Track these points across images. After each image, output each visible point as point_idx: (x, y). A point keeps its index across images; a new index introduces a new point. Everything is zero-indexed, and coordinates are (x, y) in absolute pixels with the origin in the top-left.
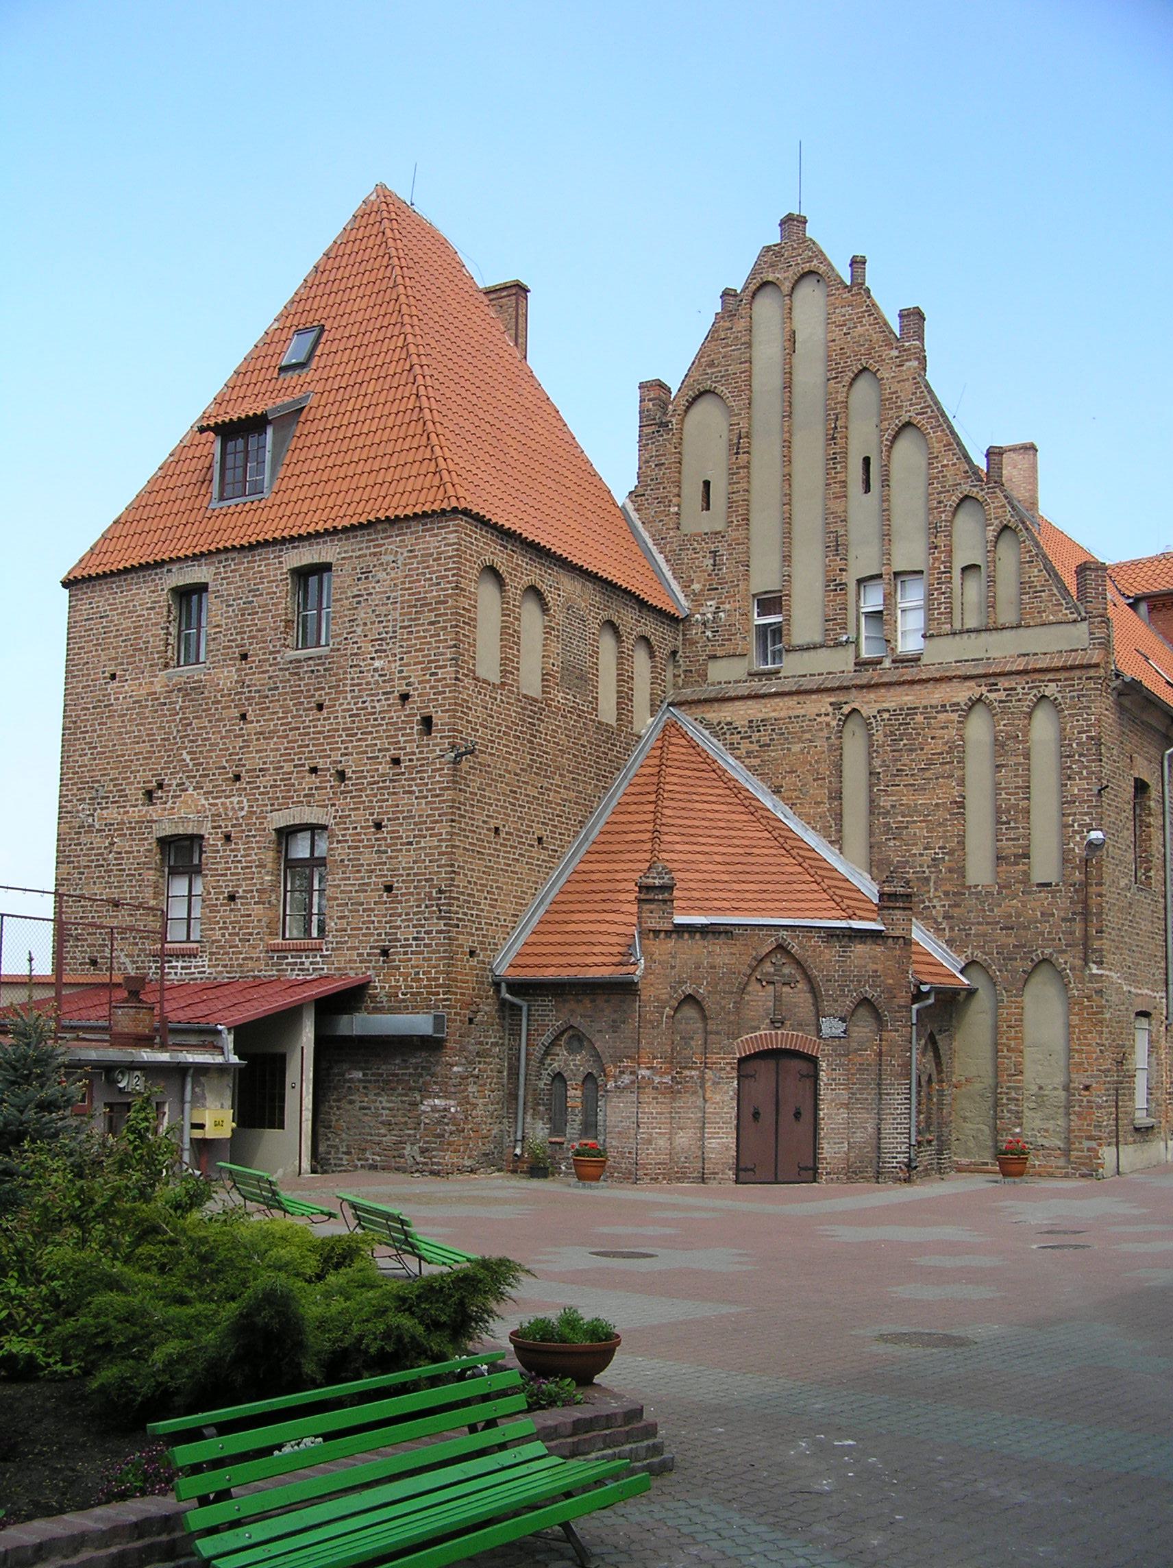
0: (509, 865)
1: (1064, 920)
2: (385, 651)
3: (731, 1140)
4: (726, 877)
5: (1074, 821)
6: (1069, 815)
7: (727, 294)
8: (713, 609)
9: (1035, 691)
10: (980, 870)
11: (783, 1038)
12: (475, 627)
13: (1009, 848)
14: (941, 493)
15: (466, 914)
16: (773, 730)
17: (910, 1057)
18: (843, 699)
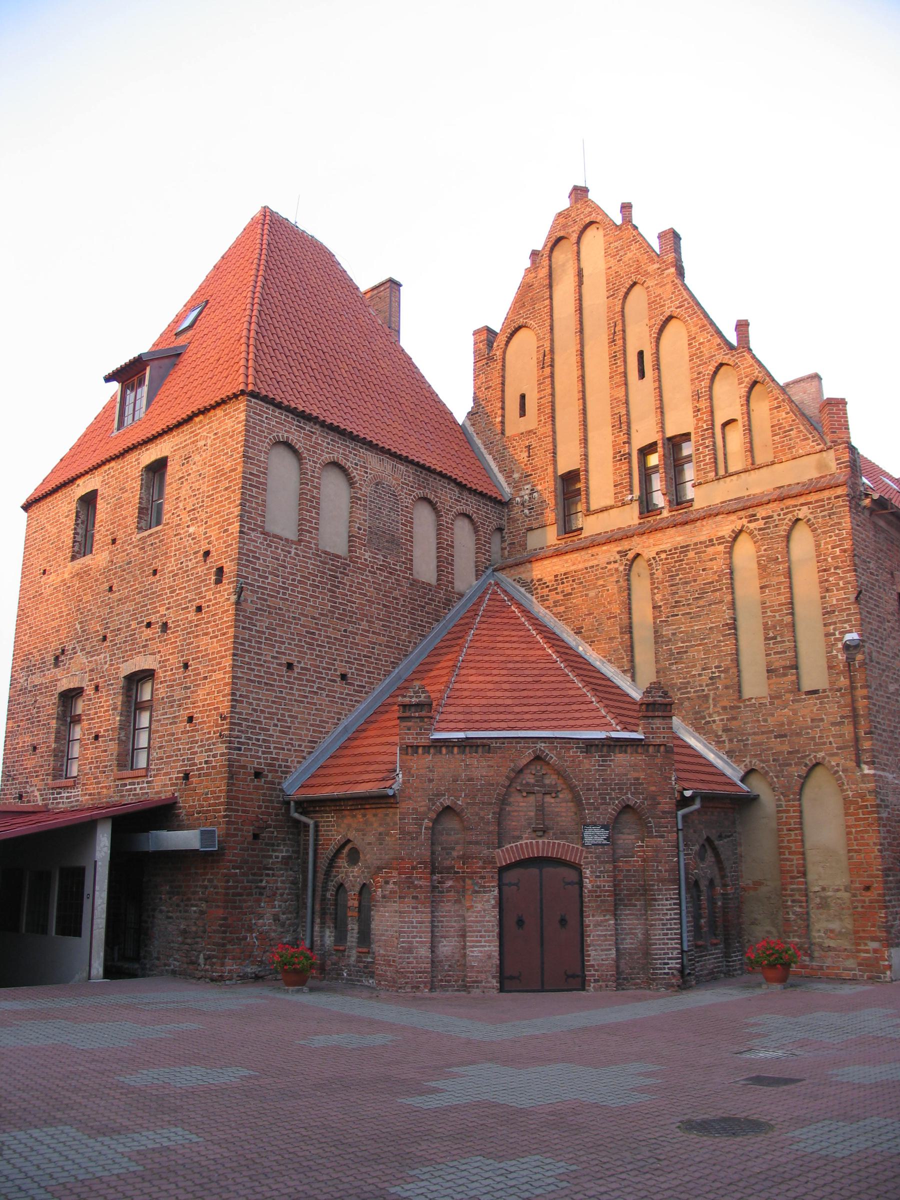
0: (306, 697)
1: (834, 724)
2: (196, 518)
3: (492, 948)
4: (509, 702)
5: (835, 629)
6: (830, 624)
7: (534, 254)
8: (528, 492)
9: (790, 516)
10: (755, 684)
11: (540, 846)
12: (265, 490)
13: (779, 662)
14: (700, 365)
15: (250, 739)
16: (573, 581)
17: (678, 862)
18: (627, 547)
